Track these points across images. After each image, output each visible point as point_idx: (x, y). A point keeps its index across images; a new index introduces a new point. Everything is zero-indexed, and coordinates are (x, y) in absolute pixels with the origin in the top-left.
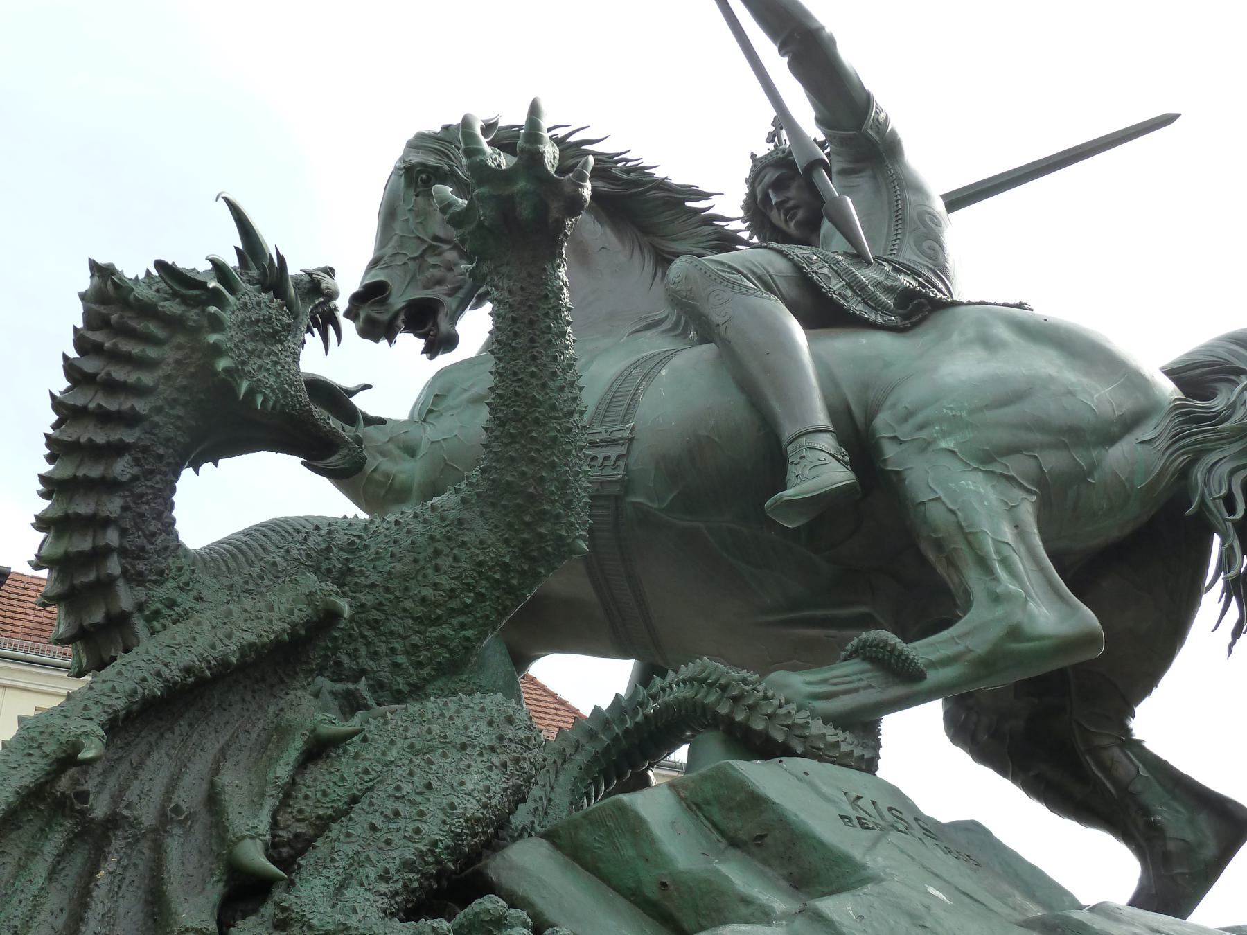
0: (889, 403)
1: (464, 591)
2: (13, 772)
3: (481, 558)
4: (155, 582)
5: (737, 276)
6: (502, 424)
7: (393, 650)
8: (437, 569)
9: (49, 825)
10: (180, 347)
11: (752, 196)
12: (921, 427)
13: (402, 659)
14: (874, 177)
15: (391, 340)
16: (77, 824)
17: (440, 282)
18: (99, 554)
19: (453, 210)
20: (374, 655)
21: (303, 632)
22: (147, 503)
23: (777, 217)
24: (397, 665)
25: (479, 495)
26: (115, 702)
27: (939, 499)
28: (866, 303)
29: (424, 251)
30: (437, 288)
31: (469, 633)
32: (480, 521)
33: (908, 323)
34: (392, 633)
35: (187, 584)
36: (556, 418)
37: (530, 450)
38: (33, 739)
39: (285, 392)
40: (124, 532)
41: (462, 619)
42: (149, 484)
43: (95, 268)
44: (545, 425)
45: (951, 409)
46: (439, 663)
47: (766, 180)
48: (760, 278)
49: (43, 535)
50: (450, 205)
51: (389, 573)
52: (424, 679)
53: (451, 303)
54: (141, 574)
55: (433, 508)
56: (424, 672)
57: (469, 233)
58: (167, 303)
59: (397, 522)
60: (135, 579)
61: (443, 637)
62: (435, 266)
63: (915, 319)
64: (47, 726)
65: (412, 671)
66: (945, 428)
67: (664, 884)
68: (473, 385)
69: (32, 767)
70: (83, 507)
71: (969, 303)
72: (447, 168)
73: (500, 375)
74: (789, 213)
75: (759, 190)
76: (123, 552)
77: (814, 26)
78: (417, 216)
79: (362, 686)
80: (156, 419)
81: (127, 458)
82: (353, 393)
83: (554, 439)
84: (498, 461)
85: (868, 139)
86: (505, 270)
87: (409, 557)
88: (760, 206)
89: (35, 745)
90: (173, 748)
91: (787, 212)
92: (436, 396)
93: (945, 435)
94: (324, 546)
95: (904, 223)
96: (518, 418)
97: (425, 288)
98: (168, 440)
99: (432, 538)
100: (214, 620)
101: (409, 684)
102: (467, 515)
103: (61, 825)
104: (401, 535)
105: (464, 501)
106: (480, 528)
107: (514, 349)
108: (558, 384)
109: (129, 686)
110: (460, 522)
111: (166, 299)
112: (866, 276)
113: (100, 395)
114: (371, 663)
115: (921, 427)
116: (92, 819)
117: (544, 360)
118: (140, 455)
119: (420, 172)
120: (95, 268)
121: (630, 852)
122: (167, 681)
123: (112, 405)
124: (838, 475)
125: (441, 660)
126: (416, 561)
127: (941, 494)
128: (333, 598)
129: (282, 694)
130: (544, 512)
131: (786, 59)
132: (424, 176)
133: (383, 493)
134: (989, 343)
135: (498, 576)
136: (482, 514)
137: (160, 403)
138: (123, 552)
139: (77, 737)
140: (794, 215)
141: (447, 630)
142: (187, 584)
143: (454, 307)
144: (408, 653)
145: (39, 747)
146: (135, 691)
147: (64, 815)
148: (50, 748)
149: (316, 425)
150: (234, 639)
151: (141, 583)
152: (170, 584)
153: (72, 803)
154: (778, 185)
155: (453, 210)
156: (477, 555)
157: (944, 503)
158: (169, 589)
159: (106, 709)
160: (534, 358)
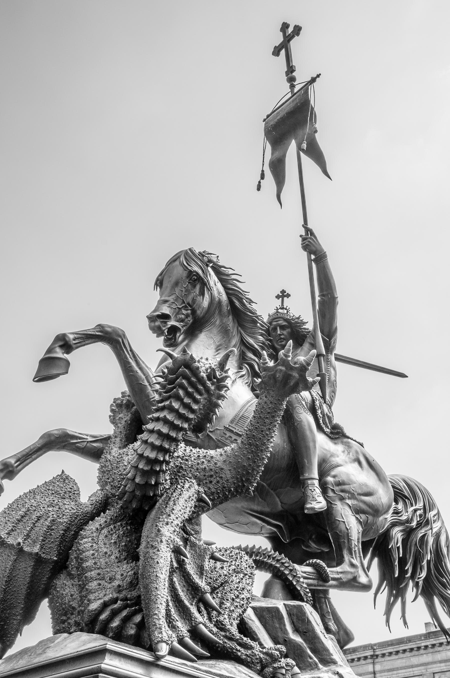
0: (333, 473)
12: (343, 491)
15: (158, 336)
27: (344, 522)
29: (183, 307)
45: (353, 490)
66: (350, 496)
67: (286, 640)
78: (186, 292)
93: (349, 498)
97: (178, 321)
115: (343, 491)
119: (194, 275)
121: (277, 626)
123: (182, 411)
127: (345, 520)
130: (249, 479)
140: (282, 341)
157: (345, 525)
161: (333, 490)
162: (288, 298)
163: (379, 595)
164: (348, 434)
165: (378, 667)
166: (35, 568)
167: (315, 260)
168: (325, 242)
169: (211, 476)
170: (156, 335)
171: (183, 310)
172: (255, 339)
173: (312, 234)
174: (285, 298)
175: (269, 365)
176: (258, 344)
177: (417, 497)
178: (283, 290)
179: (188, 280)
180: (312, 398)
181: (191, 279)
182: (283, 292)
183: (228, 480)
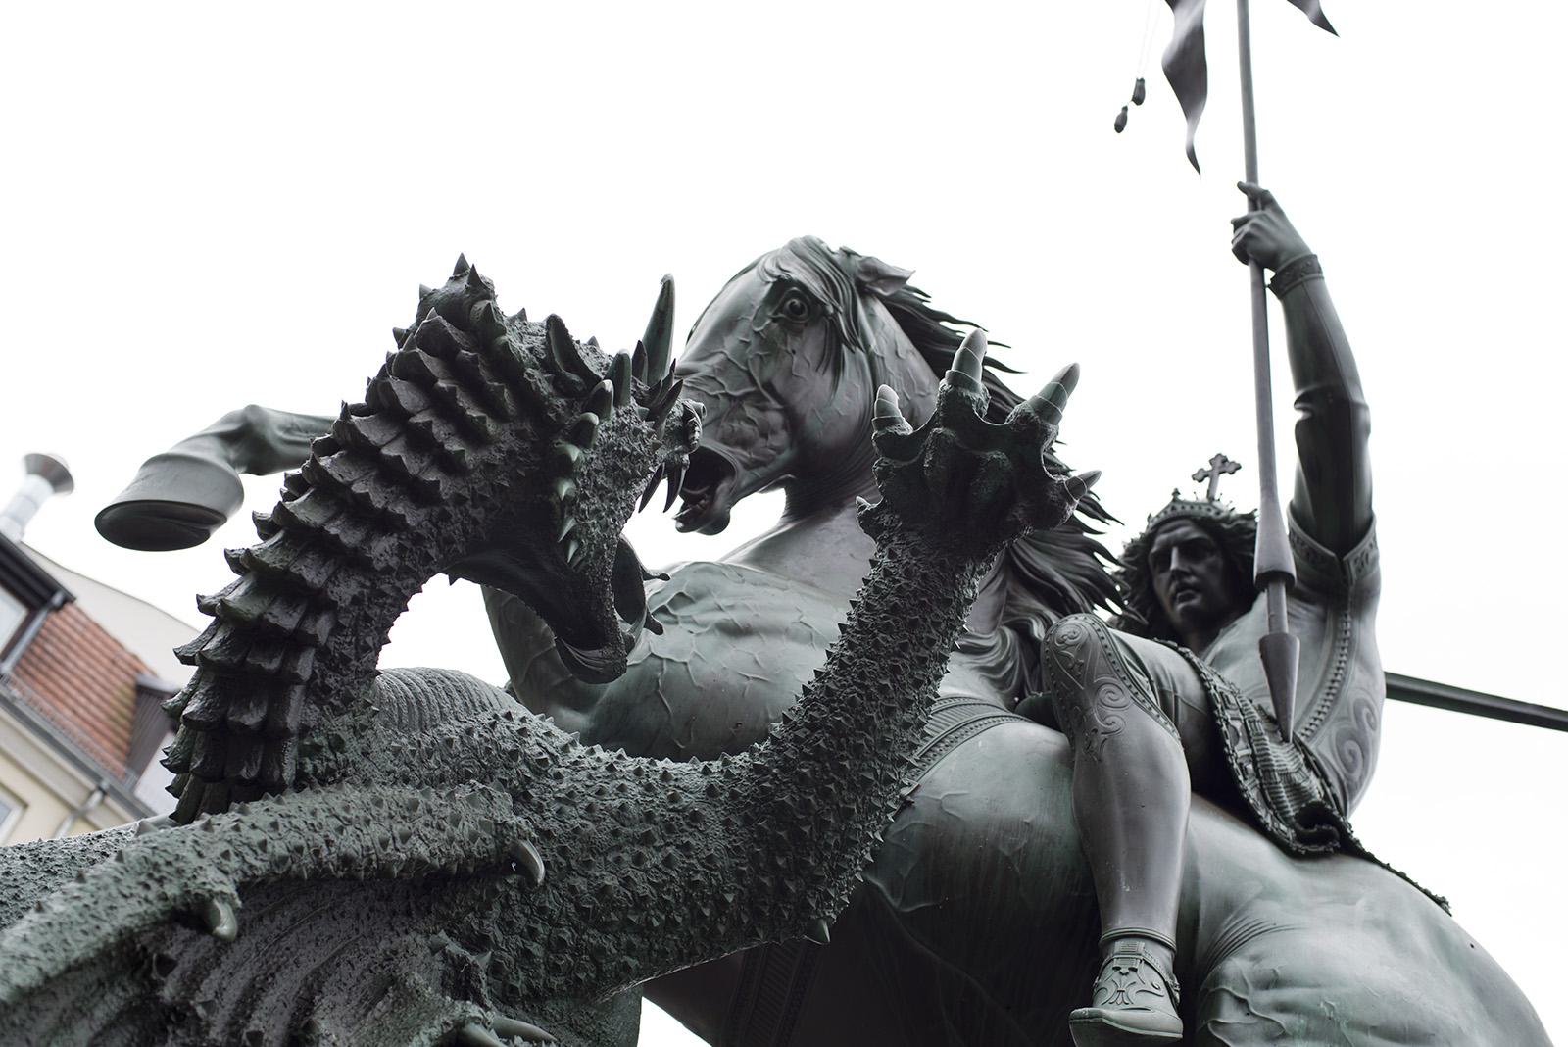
0: (1253, 948)
1: (657, 906)
2: (122, 901)
3: (698, 877)
4: (334, 708)
5: (1143, 680)
6: (813, 726)
7: (533, 934)
8: (638, 859)
9: (111, 979)
10: (520, 435)
11: (1148, 539)
12: (1283, 1008)
13: (537, 949)
14: (1323, 620)
16: (139, 996)
17: (744, 443)
18: (295, 642)
19: (891, 430)
20: (507, 926)
21: (471, 869)
22: (382, 606)
23: (1163, 585)
24: (527, 954)
25: (734, 795)
26: (258, 863)
28: (1262, 791)
29: (747, 395)
30: (739, 450)
31: (633, 962)
32: (719, 830)
33: (1303, 848)
34: (542, 910)
35: (363, 728)
36: (882, 759)
37: (832, 780)
38: (156, 866)
39: (600, 552)
40: (337, 629)
41: (636, 941)
42: (398, 584)
43: (462, 268)
44: (865, 759)
45: (1332, 1007)
46: (578, 980)
47: (1180, 532)
48: (1163, 694)
49: (236, 577)
50: (893, 422)
51: (576, 831)
52: (551, 990)
53: (744, 478)
54: (327, 690)
55: (666, 776)
56: (556, 982)
57: (898, 471)
58: (536, 373)
59: (611, 768)
60: (317, 692)
61: (601, 950)
62: (749, 421)
63: (1313, 849)
64: (178, 858)
65: (542, 971)
68: (732, 607)
69: (145, 906)
70: (311, 573)
71: (1387, 867)
72: (831, 310)
73: (842, 665)
74: (1184, 591)
75: (1162, 538)
76: (323, 653)
77: (1357, 398)
79: (483, 961)
80: (450, 509)
81: (393, 540)
82: (649, 577)
83: (866, 782)
84: (783, 770)
85: (1343, 568)
86: (912, 537)
87: (608, 823)
88: (1150, 561)
89: (157, 876)
90: (265, 941)
91: (1183, 587)
92: (681, 595)
94: (509, 746)
95: (1335, 702)
96: (837, 731)
97: (724, 441)
98: (449, 541)
99: (649, 816)
100: (394, 807)
101: (530, 987)
102: (708, 813)
103: (124, 989)
104: (610, 788)
105: (711, 791)
106: (713, 839)
107: (877, 645)
108: (906, 717)
109: (280, 849)
110: (695, 817)
111: (535, 367)
112: (1282, 757)
113: (400, 442)
114: (498, 934)
115: (1283, 1008)
116: (158, 998)
117: (906, 679)
118: (408, 545)
119: (795, 295)
120: (462, 268)
122: (320, 864)
123: (413, 466)
124: (1161, 1014)
125: (582, 977)
126: (615, 833)
128: (527, 845)
129: (400, 930)
131: (1300, 415)
132: (797, 302)
133: (557, 681)
134: (1388, 929)
135: (707, 912)
136: (727, 823)
137: (466, 493)
138: (323, 653)
139: (212, 895)
140: (1189, 597)
141: (609, 944)
142: (363, 728)
143: (744, 483)
144: (547, 946)
145: (160, 881)
146: (284, 859)
147: (132, 977)
148: (172, 890)
149: (600, 604)
150: (408, 845)
151: (320, 703)
152: (347, 718)
153: (150, 969)
154: (1189, 549)
155: (891, 430)
156: (697, 872)
158: (340, 726)
159: (245, 867)
160: (895, 670)
161: (1241, 1002)
164: (1367, 846)
167: (1275, 286)
168: (1310, 225)
171: (747, 408)
172: (1059, 558)
175: (900, 433)
176: (1067, 574)
177: (1336, 754)
179: (770, 314)
180: (1206, 690)
181: (781, 309)
183: (710, 858)
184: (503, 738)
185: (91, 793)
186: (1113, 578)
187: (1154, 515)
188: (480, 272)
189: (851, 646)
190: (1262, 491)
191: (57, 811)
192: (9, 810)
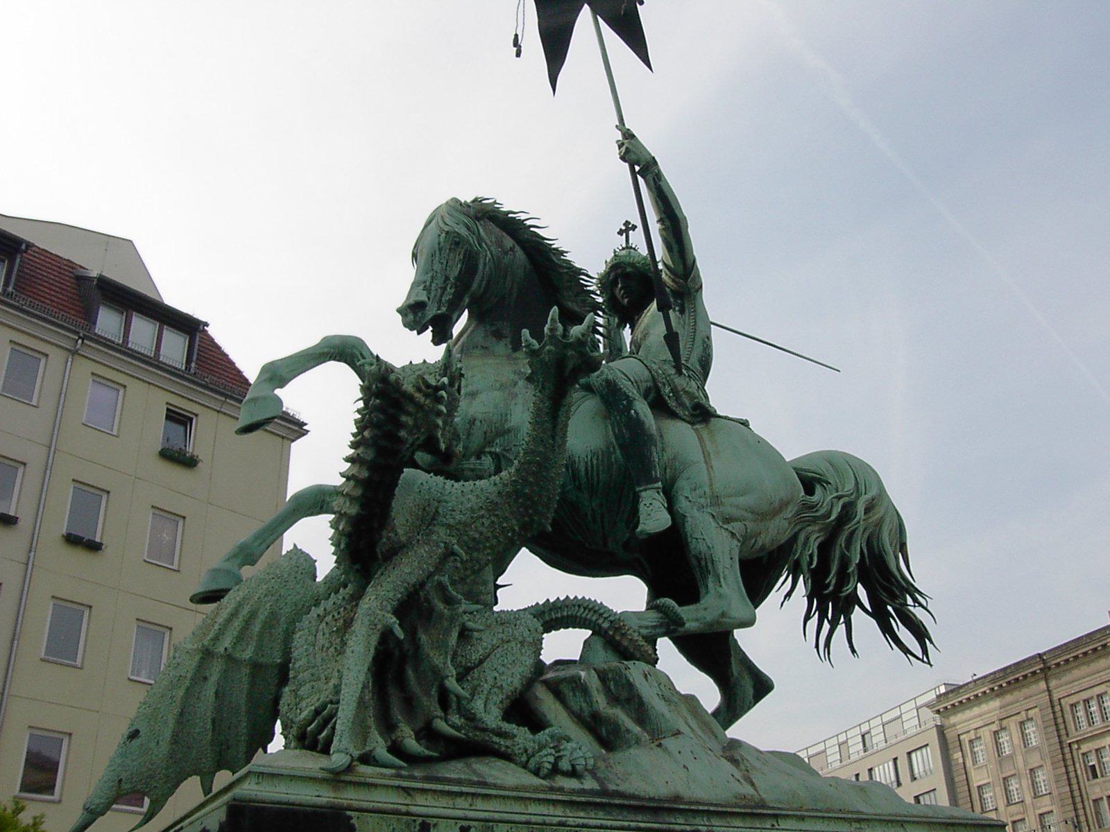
13: (459, 565)
24: (457, 568)
71: (726, 418)
148: (379, 627)
162: (634, 230)
163: (809, 623)
165: (1053, 683)
166: (253, 676)
169: (482, 517)
170: (415, 332)
173: (633, 136)
174: (631, 232)
178: (627, 221)
182: (627, 223)
184: (522, 643)
185: (77, 341)
186: (602, 304)
187: (608, 261)
188: (381, 357)
189: (534, 430)
190: (650, 245)
191: (64, 354)
192: (40, 360)
